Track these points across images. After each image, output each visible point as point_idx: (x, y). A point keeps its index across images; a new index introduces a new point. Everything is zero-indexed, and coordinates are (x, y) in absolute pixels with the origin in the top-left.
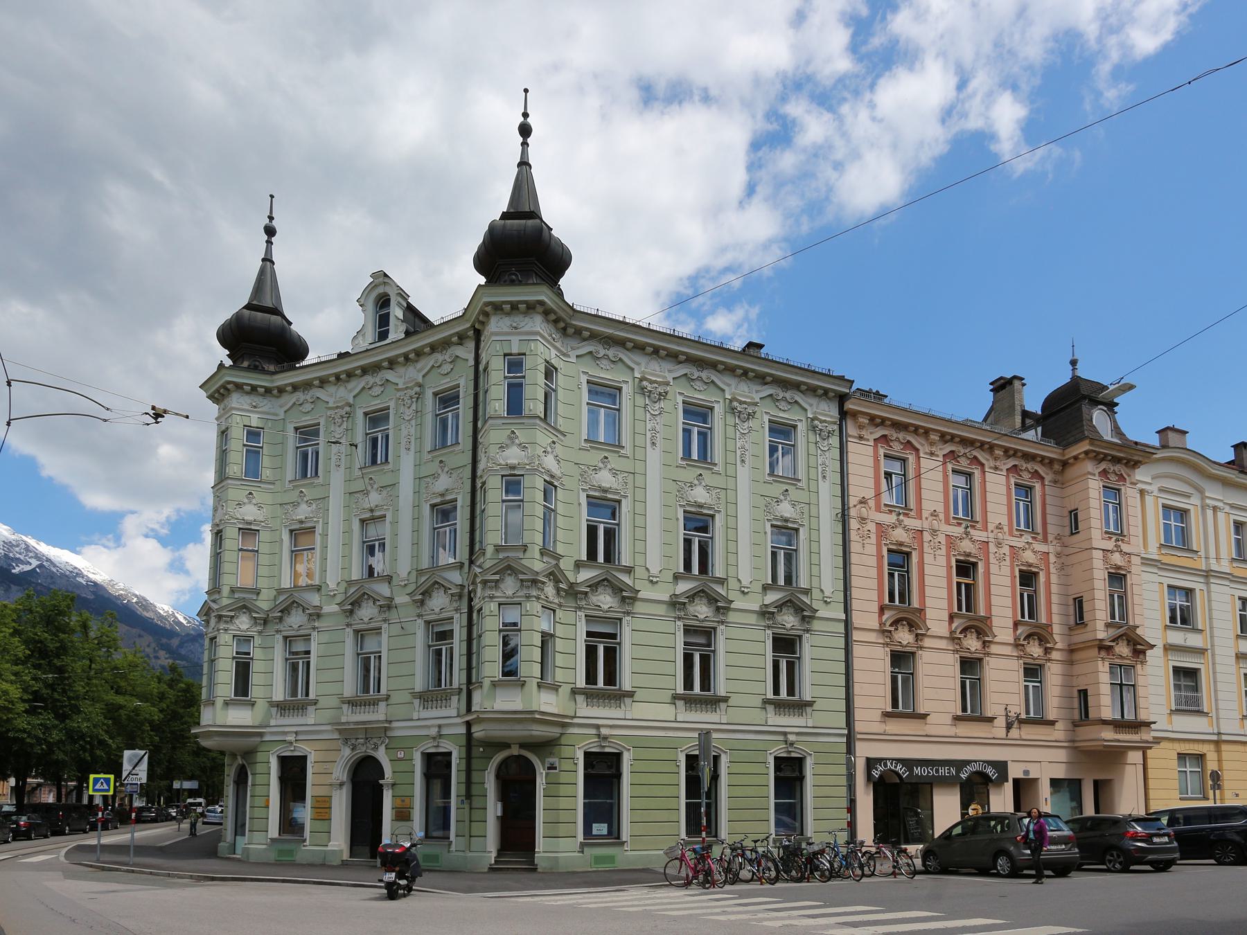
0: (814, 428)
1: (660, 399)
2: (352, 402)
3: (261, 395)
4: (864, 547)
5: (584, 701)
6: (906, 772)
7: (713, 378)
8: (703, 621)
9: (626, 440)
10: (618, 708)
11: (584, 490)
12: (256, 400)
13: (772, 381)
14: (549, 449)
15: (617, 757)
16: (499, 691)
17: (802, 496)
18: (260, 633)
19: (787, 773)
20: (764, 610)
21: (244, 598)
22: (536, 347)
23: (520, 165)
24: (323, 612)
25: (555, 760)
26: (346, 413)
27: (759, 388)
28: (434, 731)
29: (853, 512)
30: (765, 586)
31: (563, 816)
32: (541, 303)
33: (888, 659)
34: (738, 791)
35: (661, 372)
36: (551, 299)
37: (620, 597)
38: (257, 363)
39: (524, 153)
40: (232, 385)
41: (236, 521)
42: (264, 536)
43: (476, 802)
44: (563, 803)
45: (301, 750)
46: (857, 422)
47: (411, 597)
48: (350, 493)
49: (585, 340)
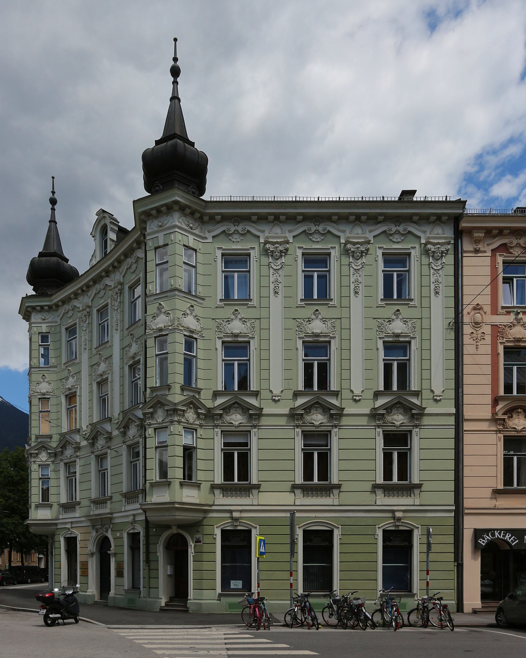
0: (427, 251)
1: (281, 256)
2: (90, 305)
3: (47, 311)
4: (477, 348)
5: (220, 493)
6: (515, 540)
7: (330, 228)
8: (319, 427)
9: (254, 295)
10: (409, 497)
11: (219, 338)
12: (45, 315)
13: (384, 219)
14: (188, 312)
15: (409, 534)
16: (155, 490)
17: (415, 313)
18: (53, 462)
19: (397, 543)
20: (374, 412)
21: (42, 441)
22: (175, 237)
23: (172, 99)
24: (81, 445)
25: (200, 536)
26: (87, 313)
27: (290, 227)
28: (130, 519)
29: (466, 319)
30: (376, 393)
31: (206, 575)
32: (176, 202)
33: (501, 444)
34: (348, 557)
35: (282, 233)
36: (183, 197)
37: (329, 415)
38: (43, 291)
39: (175, 90)
40: (29, 308)
41: (182, 328)
42: (52, 401)
43: (152, 566)
44: (206, 566)
45: (75, 534)
46: (473, 238)
47: (118, 430)
48: (91, 366)
49: (218, 222)
